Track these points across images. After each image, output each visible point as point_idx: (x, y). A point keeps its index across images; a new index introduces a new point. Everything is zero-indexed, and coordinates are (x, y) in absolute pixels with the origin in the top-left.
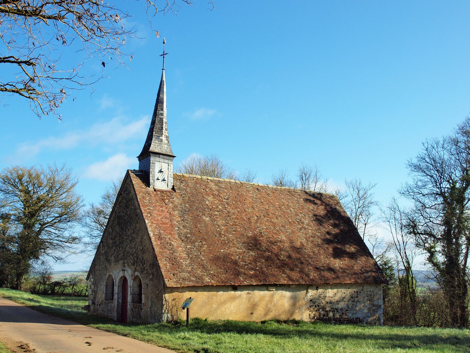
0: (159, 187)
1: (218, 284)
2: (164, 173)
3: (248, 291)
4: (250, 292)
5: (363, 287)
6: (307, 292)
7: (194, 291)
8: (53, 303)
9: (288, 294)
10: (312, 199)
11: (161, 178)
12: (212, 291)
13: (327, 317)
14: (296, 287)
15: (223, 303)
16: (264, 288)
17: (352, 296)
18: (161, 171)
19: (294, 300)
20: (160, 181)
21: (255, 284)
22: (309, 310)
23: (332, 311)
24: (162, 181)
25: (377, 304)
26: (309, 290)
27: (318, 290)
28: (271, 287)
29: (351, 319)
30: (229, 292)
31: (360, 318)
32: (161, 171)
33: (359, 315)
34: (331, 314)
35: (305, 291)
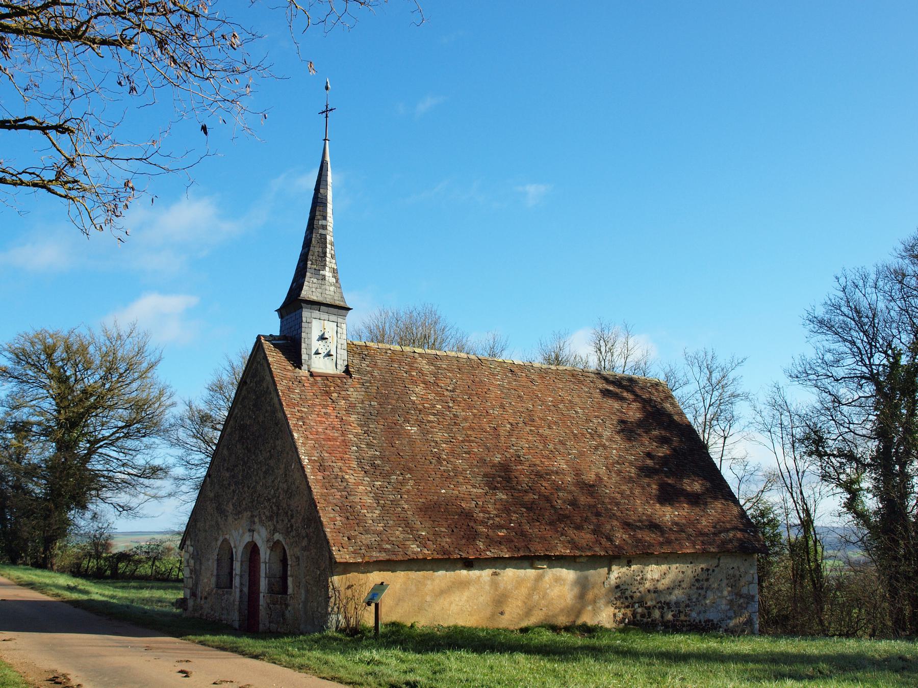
0: (319, 368)
1: (436, 556)
2: (328, 342)
4: (498, 570)
5: (719, 559)
6: (610, 570)
9: (568, 575)
11: (323, 351)
12: (423, 570)
13: (649, 619)
14: (587, 560)
16: (526, 563)
17: (696, 578)
18: (322, 338)
19: (583, 586)
21: (507, 556)
23: (659, 608)
24: (325, 356)
26: (614, 568)
27: (630, 566)
28: (538, 560)
31: (712, 620)
32: (322, 338)
33: (712, 615)
34: (657, 614)
35: (606, 569)
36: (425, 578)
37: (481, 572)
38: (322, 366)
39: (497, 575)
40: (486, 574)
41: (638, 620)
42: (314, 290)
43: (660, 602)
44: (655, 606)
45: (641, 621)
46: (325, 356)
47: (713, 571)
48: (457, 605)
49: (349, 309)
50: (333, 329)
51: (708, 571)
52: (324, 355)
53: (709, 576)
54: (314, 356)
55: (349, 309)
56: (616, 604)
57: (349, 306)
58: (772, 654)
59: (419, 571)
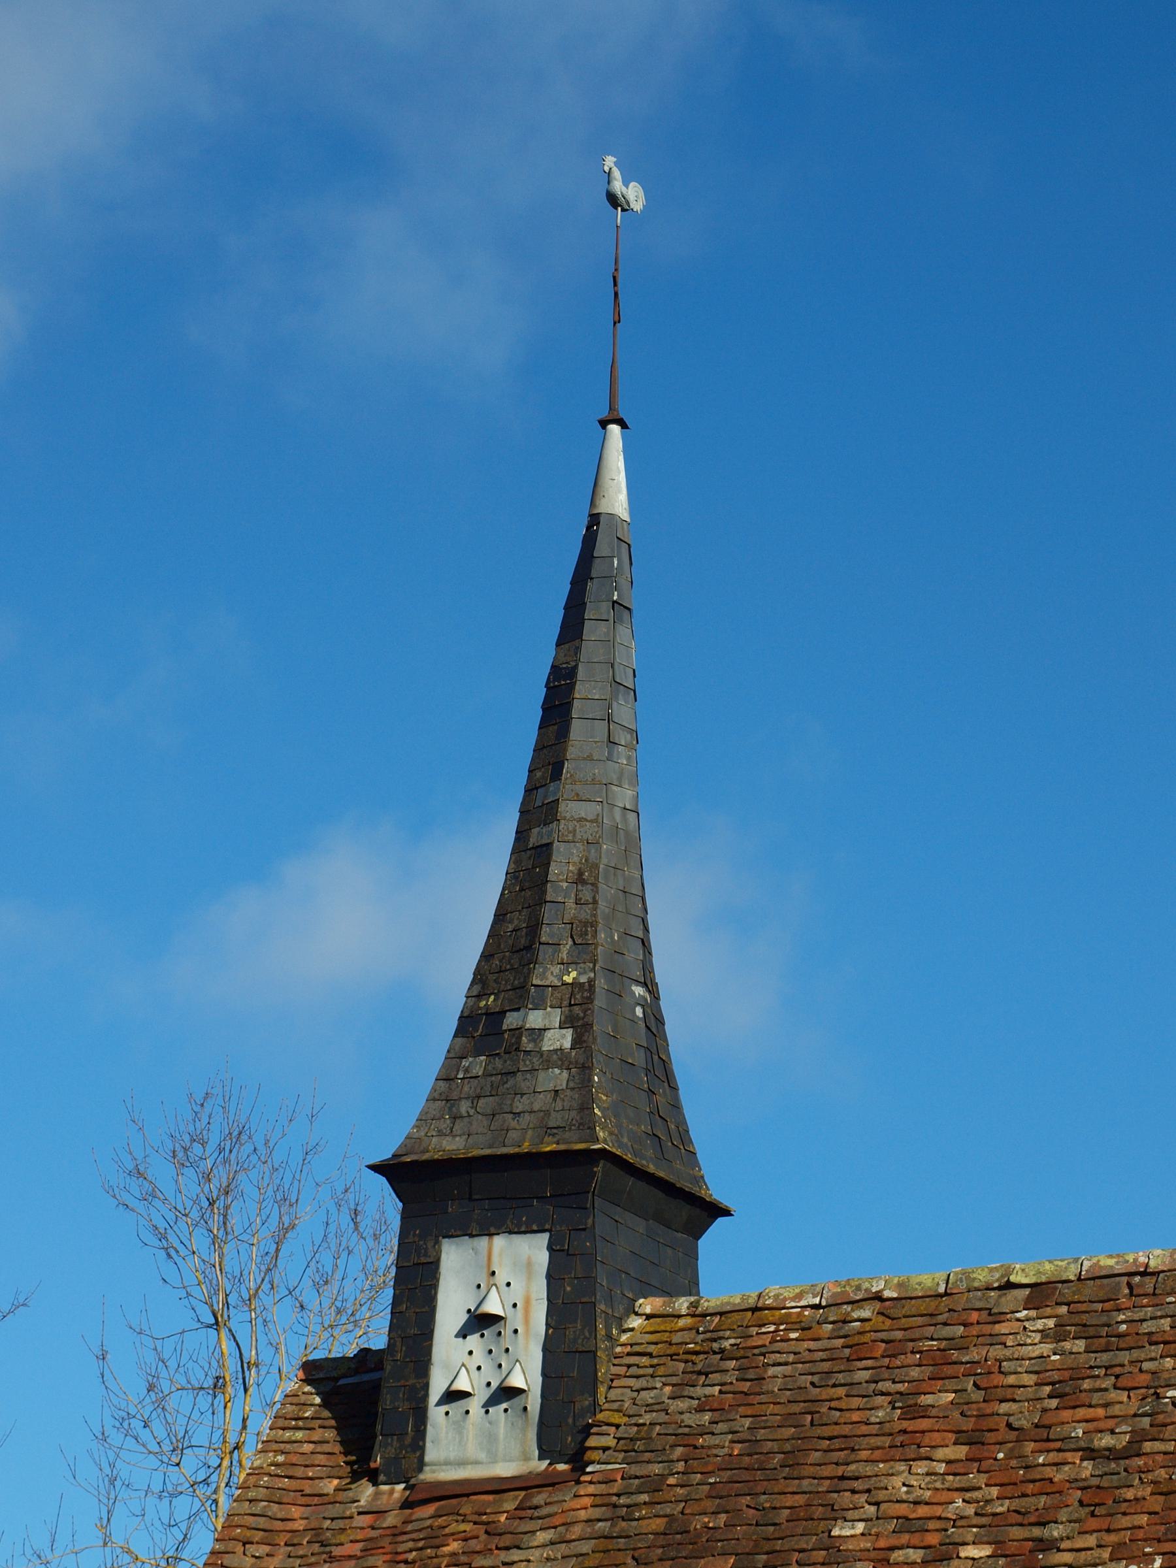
20: (475, 1405)
42: (464, 1107)
50: (529, 1264)
54: (436, 1414)
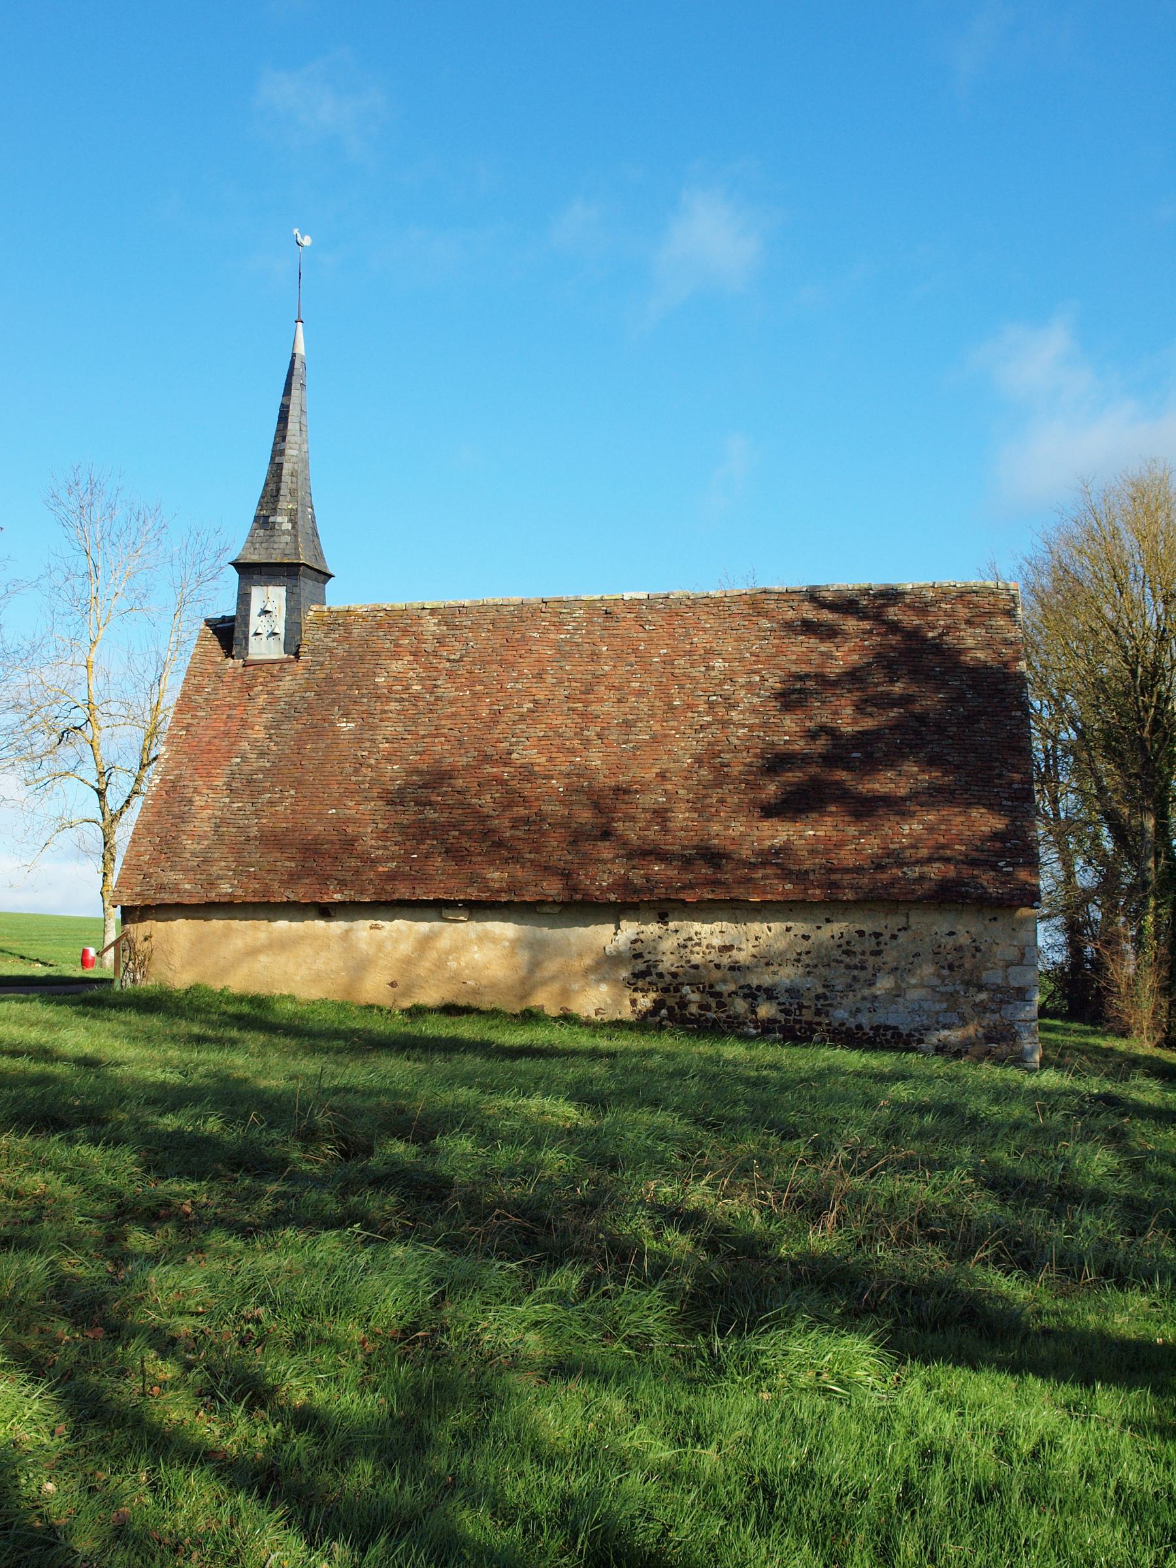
0: (261, 654)
2: (273, 616)
3: (374, 922)
4: (379, 922)
6: (618, 927)
7: (235, 919)
8: (705, 1048)
9: (505, 930)
10: (827, 616)
12: (253, 919)
15: (253, 952)
16: (432, 913)
17: (845, 947)
19: (538, 951)
21: (368, 900)
22: (633, 987)
23: (745, 997)
24: (269, 636)
25: (999, 981)
26: (624, 924)
27: (666, 923)
28: (447, 908)
29: (848, 1029)
30: (308, 923)
31: (896, 1028)
33: (897, 1017)
34: (740, 1006)
35: (612, 927)
36: (230, 929)
37: (350, 924)
38: (263, 650)
39: (379, 928)
40: (337, 926)
41: (691, 1014)
43: (749, 987)
44: (735, 993)
45: (701, 1015)
46: (269, 636)
47: (894, 937)
48: (310, 969)
49: (330, 576)
51: (877, 938)
52: (267, 634)
53: (882, 947)
55: (330, 576)
56: (634, 984)
57: (331, 571)
58: (408, 1036)
59: (246, 919)
